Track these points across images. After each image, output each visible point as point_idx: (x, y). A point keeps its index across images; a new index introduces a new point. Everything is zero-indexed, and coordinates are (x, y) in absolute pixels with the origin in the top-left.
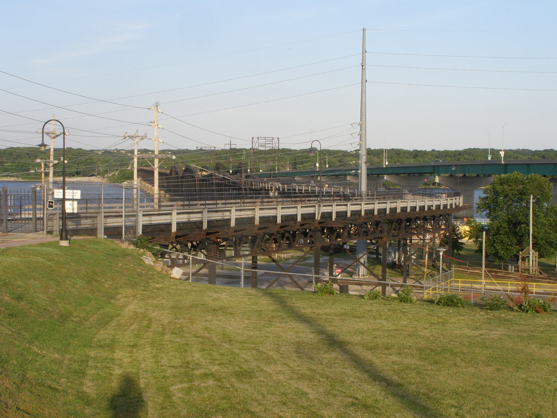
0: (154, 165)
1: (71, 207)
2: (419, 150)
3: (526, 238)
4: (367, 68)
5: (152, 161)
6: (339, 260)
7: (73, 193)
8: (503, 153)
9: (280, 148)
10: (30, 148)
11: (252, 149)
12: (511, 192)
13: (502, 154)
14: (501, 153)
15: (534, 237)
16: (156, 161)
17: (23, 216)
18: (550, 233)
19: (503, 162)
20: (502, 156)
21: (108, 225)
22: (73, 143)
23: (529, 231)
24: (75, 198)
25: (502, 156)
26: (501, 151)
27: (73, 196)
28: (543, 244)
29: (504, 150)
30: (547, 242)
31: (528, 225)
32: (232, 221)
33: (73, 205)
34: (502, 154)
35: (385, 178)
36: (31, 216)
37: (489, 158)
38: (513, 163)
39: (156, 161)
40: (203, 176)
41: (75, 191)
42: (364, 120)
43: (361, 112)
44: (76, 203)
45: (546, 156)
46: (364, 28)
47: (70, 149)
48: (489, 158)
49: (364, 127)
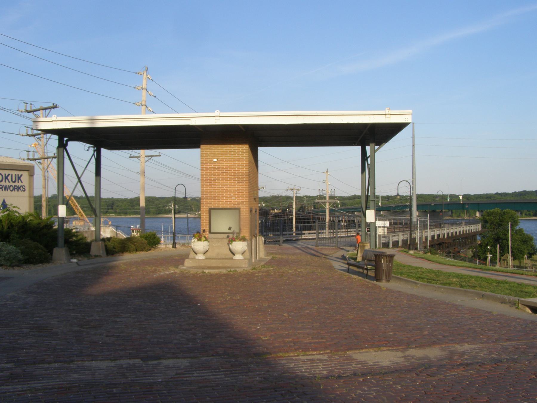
0: (326, 206)
1: (383, 231)
2: (390, 195)
3: (506, 248)
4: (416, 146)
5: (325, 205)
6: (460, 263)
7: (384, 223)
8: (462, 196)
9: (336, 195)
10: (153, 197)
11: (398, 195)
12: (495, 220)
13: (461, 197)
14: (460, 196)
15: (511, 248)
16: (327, 204)
17: (302, 238)
18: (520, 245)
19: (461, 203)
20: (461, 198)
21: (394, 240)
22: (302, 194)
23: (508, 244)
24: (385, 226)
25: (461, 198)
26: (460, 195)
27: (384, 225)
28: (516, 252)
29: (462, 195)
30: (519, 251)
31: (508, 241)
32: (417, 239)
33: (384, 230)
34: (461, 197)
35: (356, 214)
36: (315, 237)
37: (448, 200)
38: (490, 202)
39: (327, 204)
40: (276, 213)
41: (385, 222)
42: (414, 178)
43: (413, 173)
44: (386, 229)
45: (469, 198)
46: (56, 103)
47: (177, 197)
48: (448, 200)
49: (414, 182)
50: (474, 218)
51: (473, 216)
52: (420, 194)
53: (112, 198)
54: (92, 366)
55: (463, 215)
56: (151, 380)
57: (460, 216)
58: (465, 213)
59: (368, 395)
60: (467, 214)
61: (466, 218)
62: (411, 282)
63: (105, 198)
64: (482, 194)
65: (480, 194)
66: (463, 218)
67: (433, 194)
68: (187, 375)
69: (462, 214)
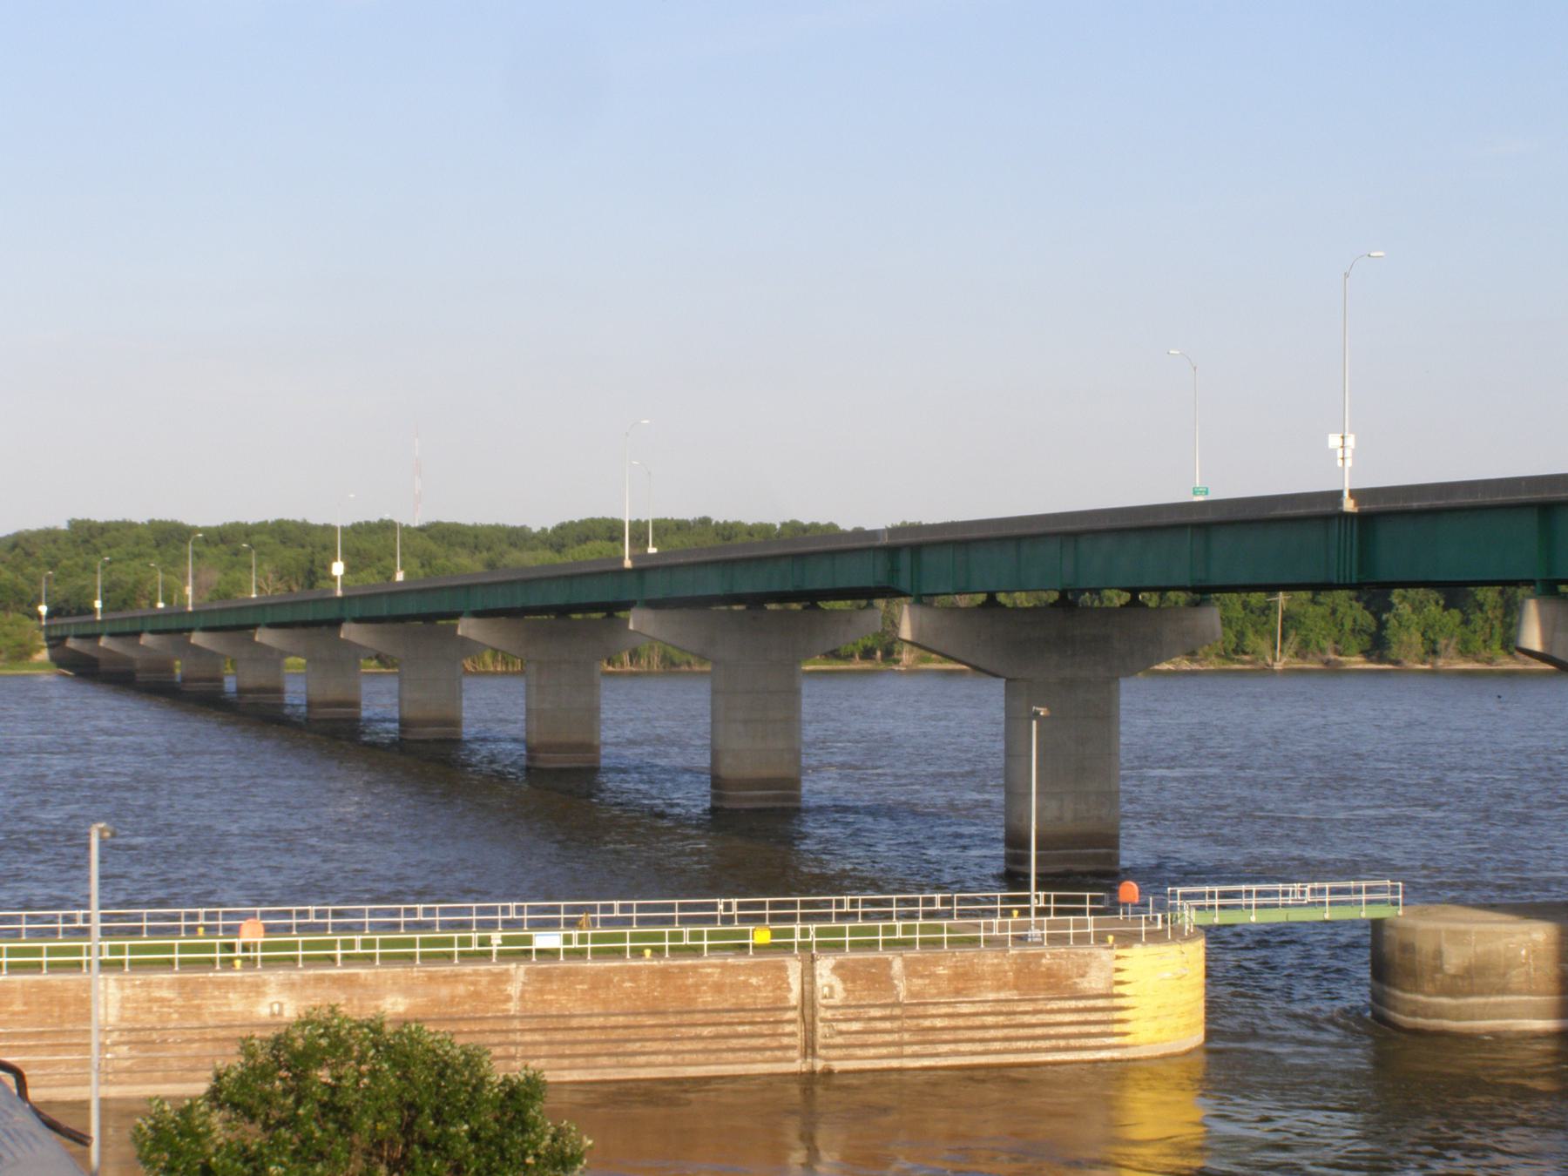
48: (400, 576)
50: (1328, 663)
51: (1322, 651)
52: (750, 523)
53: (832, 526)
54: (1200, 908)
55: (1264, 645)
56: (1506, 895)
57: (1239, 650)
58: (1273, 633)
59: (1359, 1028)
60: (1284, 638)
61: (1278, 666)
62: (19, 1047)
63: (870, 525)
64: (482, 527)
65: (541, 517)
66: (1261, 664)
67: (442, 524)
68: (636, 1046)
69: (1251, 640)
